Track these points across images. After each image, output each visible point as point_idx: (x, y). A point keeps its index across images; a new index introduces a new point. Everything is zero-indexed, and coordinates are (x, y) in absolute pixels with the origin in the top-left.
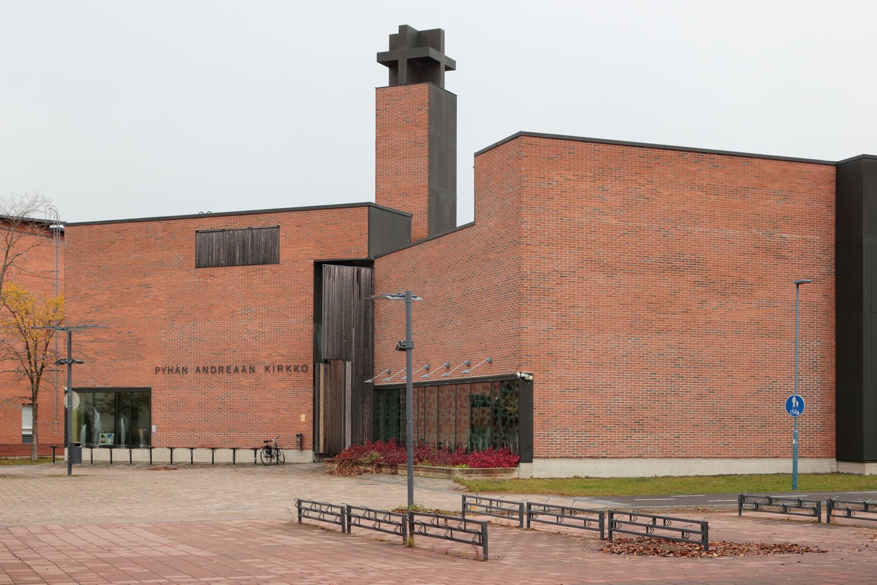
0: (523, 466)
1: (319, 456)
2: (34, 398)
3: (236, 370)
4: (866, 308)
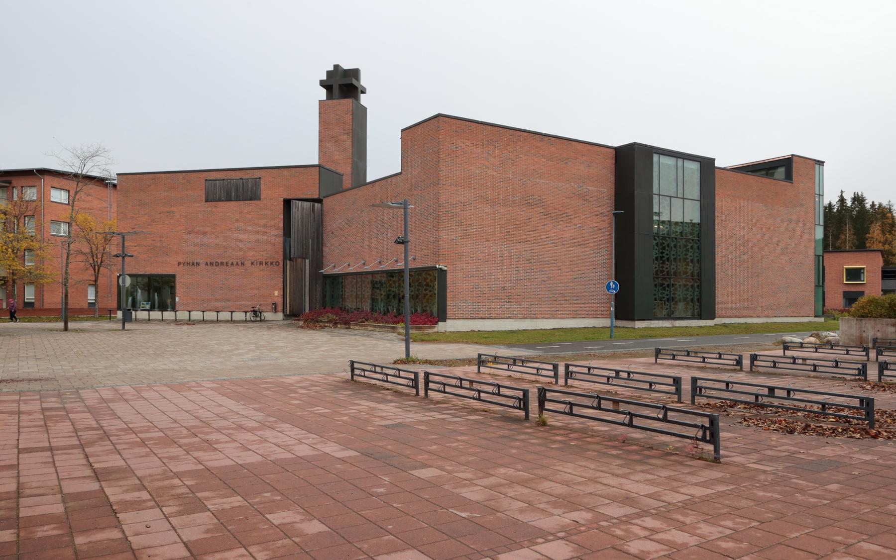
0: (440, 324)
1: (287, 317)
2: (96, 281)
3: (232, 264)
4: (636, 232)
